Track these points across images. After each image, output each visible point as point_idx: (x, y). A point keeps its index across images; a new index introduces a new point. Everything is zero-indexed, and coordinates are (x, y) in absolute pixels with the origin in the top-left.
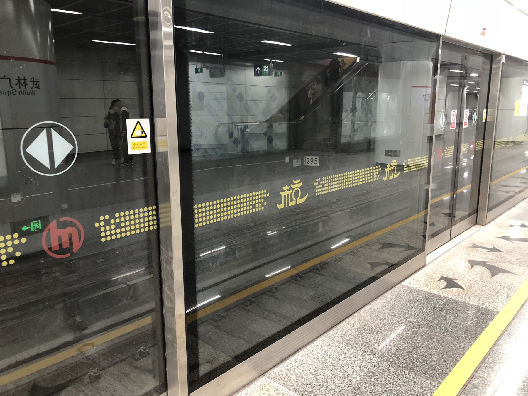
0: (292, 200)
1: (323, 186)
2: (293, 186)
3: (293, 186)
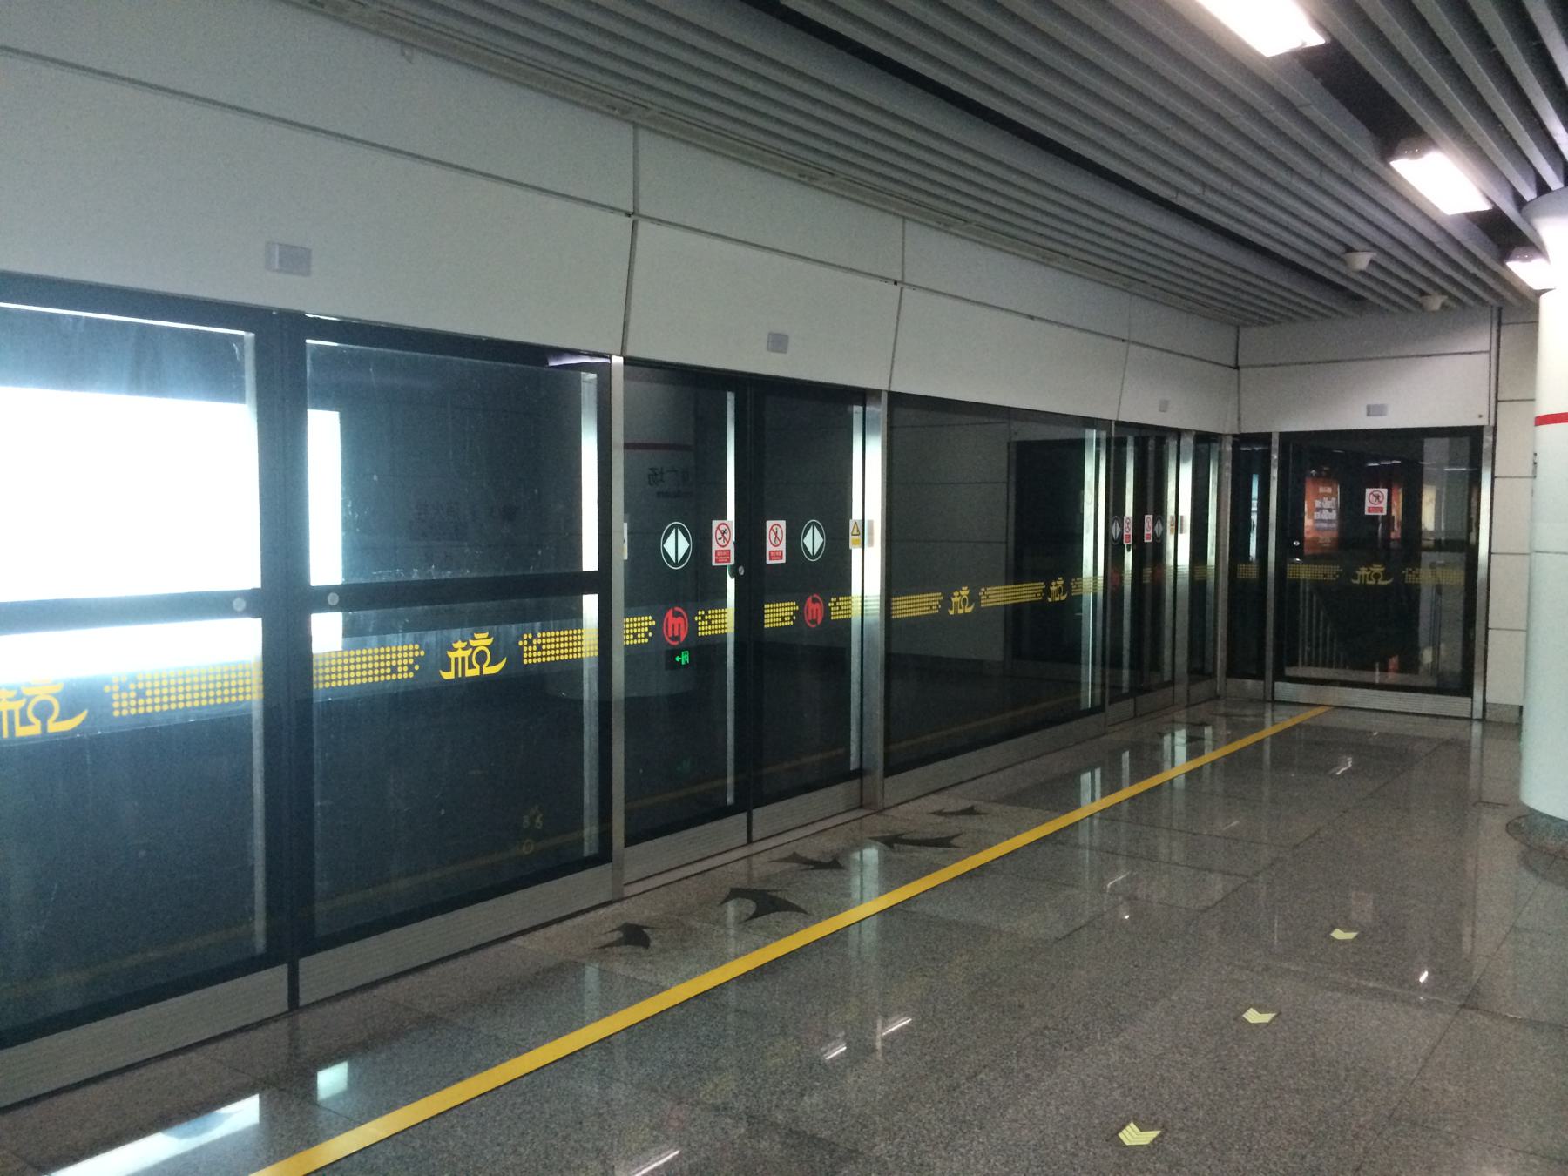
0: (471, 666)
1: (539, 648)
2: (473, 643)
3: (473, 643)
